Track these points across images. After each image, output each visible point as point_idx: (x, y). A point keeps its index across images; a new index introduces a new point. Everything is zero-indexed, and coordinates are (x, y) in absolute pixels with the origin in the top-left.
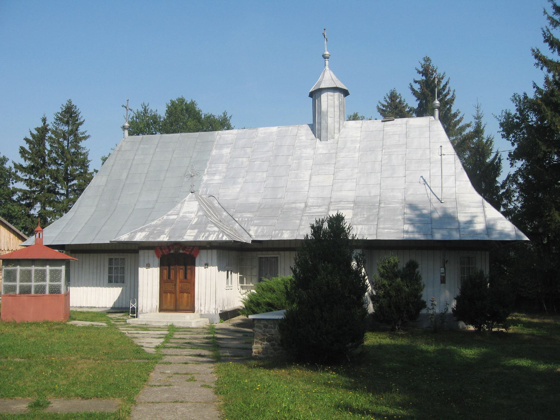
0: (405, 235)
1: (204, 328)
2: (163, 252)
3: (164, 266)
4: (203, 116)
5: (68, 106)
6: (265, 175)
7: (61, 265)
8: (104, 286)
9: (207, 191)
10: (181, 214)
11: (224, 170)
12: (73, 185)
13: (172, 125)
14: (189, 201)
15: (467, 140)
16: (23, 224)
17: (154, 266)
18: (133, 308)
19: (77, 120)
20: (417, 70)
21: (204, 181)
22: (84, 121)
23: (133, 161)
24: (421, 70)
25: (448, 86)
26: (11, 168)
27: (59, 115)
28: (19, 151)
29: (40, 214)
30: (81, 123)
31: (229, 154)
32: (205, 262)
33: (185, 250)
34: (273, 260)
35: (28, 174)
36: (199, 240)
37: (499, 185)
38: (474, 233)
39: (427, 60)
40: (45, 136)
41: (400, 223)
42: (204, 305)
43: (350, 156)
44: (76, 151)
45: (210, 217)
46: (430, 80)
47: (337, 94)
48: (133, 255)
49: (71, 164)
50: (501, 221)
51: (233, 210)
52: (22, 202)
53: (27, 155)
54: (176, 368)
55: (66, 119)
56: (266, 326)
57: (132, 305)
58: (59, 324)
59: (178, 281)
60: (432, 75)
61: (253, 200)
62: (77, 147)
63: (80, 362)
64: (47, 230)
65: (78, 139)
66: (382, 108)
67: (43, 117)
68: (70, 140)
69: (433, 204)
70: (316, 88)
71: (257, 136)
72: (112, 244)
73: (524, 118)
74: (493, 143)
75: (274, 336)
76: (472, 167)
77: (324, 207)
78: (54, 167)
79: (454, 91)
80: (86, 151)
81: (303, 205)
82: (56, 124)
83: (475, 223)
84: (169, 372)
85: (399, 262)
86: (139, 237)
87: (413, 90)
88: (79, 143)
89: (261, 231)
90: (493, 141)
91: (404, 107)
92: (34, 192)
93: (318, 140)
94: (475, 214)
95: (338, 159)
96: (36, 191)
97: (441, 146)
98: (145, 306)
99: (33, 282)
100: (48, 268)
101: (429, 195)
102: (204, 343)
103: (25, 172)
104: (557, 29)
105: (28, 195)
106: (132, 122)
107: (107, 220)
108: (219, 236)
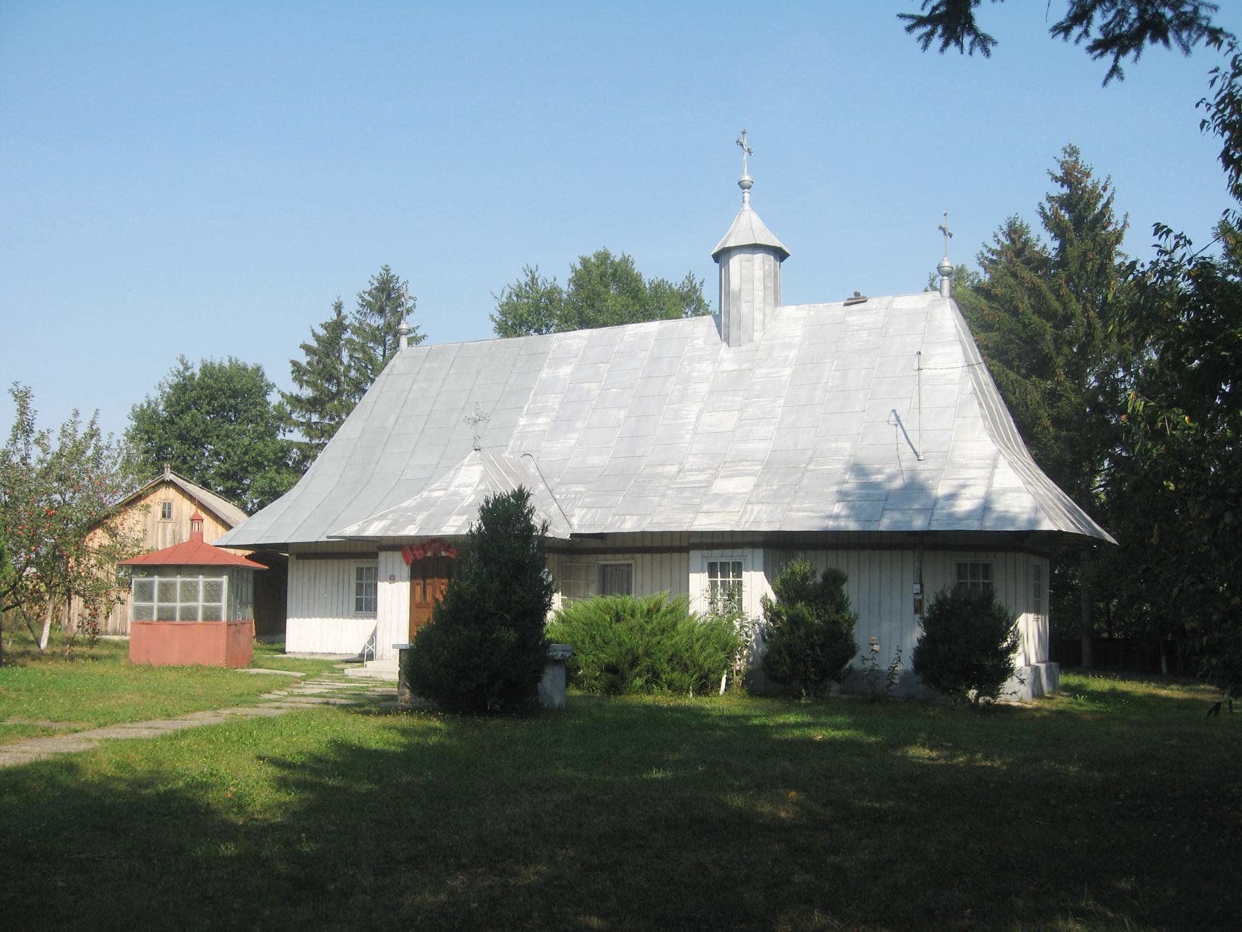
2: (414, 555)
3: (416, 579)
7: (220, 575)
8: (349, 617)
9: (521, 445)
11: (557, 406)
17: (401, 580)
20: (1051, 174)
23: (409, 393)
24: (1059, 173)
32: (390, 573)
33: (448, 551)
34: (626, 570)
39: (1073, 151)
43: (774, 375)
47: (759, 257)
51: (556, 479)
61: (595, 460)
66: (991, 257)
81: (675, 469)
89: (591, 517)
93: (724, 345)
100: (201, 579)
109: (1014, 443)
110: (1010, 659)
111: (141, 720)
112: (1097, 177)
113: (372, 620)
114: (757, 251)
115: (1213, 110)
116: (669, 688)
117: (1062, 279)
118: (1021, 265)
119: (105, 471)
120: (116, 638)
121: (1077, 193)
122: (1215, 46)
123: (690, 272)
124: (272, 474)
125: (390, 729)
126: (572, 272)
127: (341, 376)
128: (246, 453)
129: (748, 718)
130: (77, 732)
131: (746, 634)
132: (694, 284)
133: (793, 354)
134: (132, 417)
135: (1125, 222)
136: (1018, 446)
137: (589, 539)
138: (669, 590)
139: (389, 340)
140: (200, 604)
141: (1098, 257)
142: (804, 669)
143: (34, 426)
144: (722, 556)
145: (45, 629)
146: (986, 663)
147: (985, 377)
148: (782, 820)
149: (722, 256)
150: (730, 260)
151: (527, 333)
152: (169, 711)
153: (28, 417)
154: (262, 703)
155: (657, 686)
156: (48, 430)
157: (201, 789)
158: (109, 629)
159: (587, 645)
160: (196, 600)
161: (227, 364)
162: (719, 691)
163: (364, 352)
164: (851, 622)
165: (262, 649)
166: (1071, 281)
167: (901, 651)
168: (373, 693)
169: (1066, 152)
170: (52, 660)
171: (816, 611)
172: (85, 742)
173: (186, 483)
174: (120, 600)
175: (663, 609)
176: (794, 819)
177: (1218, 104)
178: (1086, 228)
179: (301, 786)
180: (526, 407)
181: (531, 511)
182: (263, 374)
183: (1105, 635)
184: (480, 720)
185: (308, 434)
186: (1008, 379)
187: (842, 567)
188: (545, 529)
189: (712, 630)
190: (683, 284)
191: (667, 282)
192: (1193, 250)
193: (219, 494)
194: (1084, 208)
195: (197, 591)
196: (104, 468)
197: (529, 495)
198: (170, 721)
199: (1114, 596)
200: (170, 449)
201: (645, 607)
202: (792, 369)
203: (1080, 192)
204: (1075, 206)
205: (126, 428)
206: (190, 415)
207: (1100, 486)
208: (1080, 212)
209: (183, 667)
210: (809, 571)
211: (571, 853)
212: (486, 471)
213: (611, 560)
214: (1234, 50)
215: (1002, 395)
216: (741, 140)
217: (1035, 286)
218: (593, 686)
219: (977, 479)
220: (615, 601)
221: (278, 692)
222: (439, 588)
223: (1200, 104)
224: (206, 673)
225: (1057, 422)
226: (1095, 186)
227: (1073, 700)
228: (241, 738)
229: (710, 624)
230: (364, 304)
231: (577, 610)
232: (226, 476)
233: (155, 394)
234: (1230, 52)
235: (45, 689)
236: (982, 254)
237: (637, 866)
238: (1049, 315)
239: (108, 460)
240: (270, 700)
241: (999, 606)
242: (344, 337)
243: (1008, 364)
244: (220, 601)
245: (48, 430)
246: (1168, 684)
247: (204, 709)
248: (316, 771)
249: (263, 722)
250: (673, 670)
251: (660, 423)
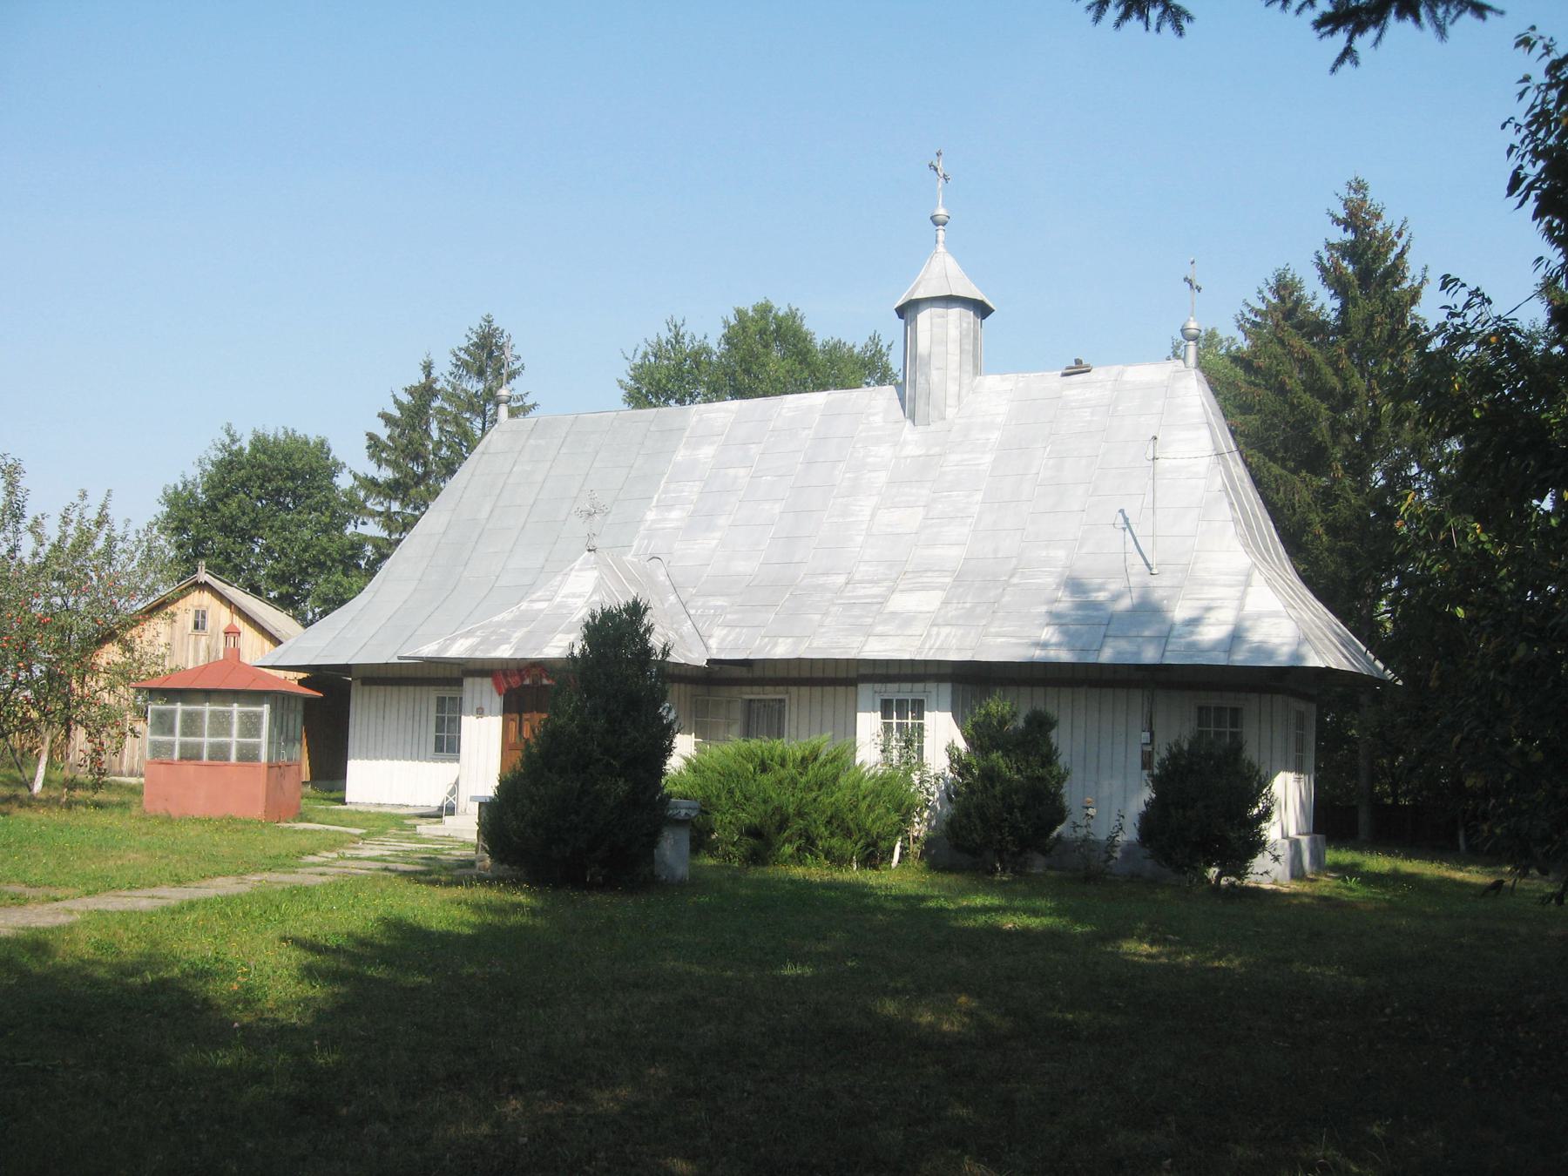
2: (508, 683)
3: (510, 712)
7: (260, 703)
9: (647, 548)
10: (558, 600)
11: (694, 497)
17: (491, 714)
20: (1331, 215)
24: (1342, 214)
32: (477, 705)
34: (777, 706)
39: (1360, 187)
47: (955, 312)
61: (741, 566)
66: (1254, 318)
67: (425, 359)
70: (907, 300)
76: (1457, 471)
81: (841, 579)
86: (458, 649)
93: (909, 423)
100: (236, 709)
109: (1274, 555)
110: (1261, 830)
111: (142, 886)
112: (1390, 219)
113: (456, 763)
114: (954, 305)
115: (1524, 132)
116: (826, 858)
117: (1341, 348)
118: (1290, 329)
119: (119, 568)
120: (133, 780)
121: (1364, 240)
122: (1524, 52)
123: (875, 331)
124: (338, 577)
125: (459, 904)
126: (725, 327)
127: (430, 454)
128: (305, 550)
129: (923, 898)
130: (57, 900)
131: (927, 790)
132: (879, 347)
133: (995, 436)
134: (163, 502)
135: (1424, 278)
136: (1280, 559)
137: (733, 667)
138: (830, 734)
139: (490, 410)
140: (234, 739)
141: (1388, 321)
142: (999, 837)
143: (25, 509)
144: (899, 692)
145: (40, 767)
146: (1231, 834)
147: (1240, 471)
148: (944, 1035)
149: (908, 310)
150: (918, 316)
151: (666, 403)
152: (181, 875)
153: (18, 498)
154: (302, 868)
155: (811, 855)
156: (42, 515)
157: (200, 979)
158: (125, 769)
159: (723, 801)
160: (229, 734)
161: (281, 436)
162: (890, 862)
163: (458, 425)
164: (1061, 779)
165: (316, 798)
166: (1354, 351)
167: (1123, 817)
168: (448, 857)
169: (1351, 187)
170: (44, 806)
172: (65, 914)
173: (225, 586)
174: (134, 732)
175: (822, 758)
176: (959, 1033)
177: (1529, 125)
178: (1374, 285)
179: (333, 976)
180: (655, 500)
181: (649, 630)
182: (329, 449)
183: (1390, 801)
184: (575, 895)
185: (386, 526)
186: (1271, 474)
187: (1051, 709)
188: (666, 652)
189: (883, 785)
190: (866, 347)
191: (844, 344)
192: (1499, 308)
193: (271, 602)
194: (1372, 258)
195: (230, 724)
196: (119, 564)
197: (646, 609)
198: (180, 889)
199: (1399, 751)
200: (210, 542)
201: (799, 755)
202: (994, 456)
203: (1368, 239)
204: (1362, 256)
205: (155, 516)
206: (236, 500)
207: (1386, 612)
208: (1367, 264)
209: (210, 820)
210: (1009, 712)
211: (661, 1073)
212: (602, 578)
213: (759, 694)
214: (1551, 54)
215: (1261, 495)
216: (935, 163)
217: (1306, 357)
218: (730, 853)
219: (1226, 599)
220: (761, 746)
221: (326, 854)
222: (534, 721)
223: (1508, 125)
224: (239, 827)
225: (1332, 529)
226: (1387, 232)
227: (1342, 883)
228: (265, 913)
229: (881, 777)
230: (460, 363)
231: (712, 757)
232: (279, 578)
233: (193, 473)
234: (1546, 57)
235: (26, 844)
236: (1243, 315)
237: (744, 1091)
238: (1325, 394)
239: (124, 554)
240: (314, 864)
241: (1249, 762)
242: (434, 405)
243: (1271, 456)
244: (259, 737)
245: (42, 515)
246: (1466, 865)
247: (225, 874)
248: (355, 958)
249: (295, 893)
250: (832, 835)
251: (824, 520)
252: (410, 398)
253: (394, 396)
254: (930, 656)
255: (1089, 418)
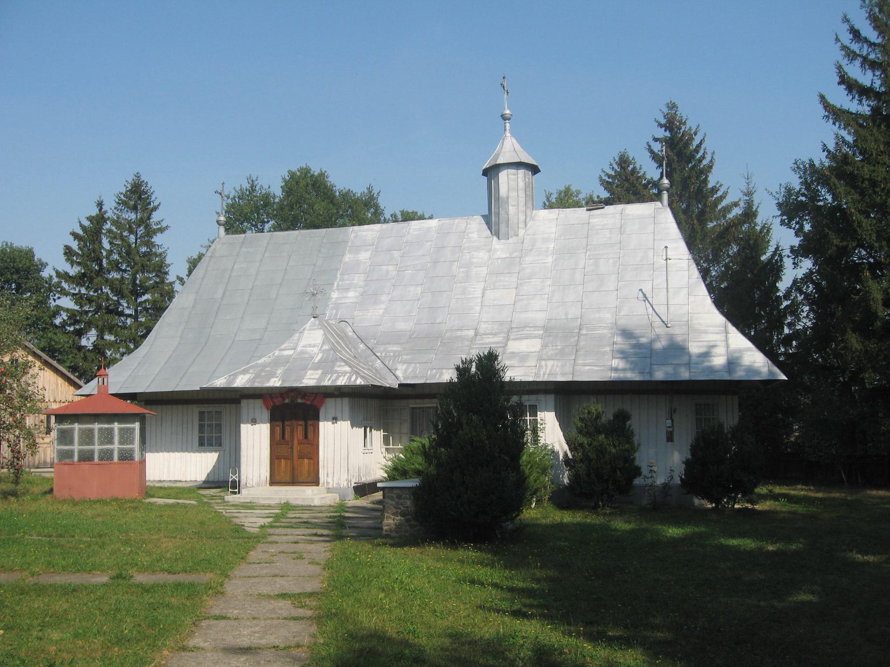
0: (613, 375)
1: (330, 506)
2: (274, 402)
3: (276, 421)
4: (337, 194)
5: (135, 183)
6: (419, 290)
7: (134, 422)
10: (299, 349)
11: (362, 283)
12: (145, 301)
13: (292, 209)
14: (310, 330)
15: (732, 227)
16: (71, 362)
17: (262, 422)
18: (234, 482)
19: (149, 204)
20: (657, 122)
21: (334, 300)
22: (159, 205)
23: (231, 272)
24: (663, 121)
25: (703, 146)
26: (51, 277)
27: (122, 196)
28: (63, 252)
29: (95, 346)
30: (155, 209)
31: (368, 260)
32: (333, 415)
33: (305, 399)
35: (77, 285)
36: (324, 384)
37: (780, 294)
38: (711, 369)
39: (672, 106)
40: (101, 228)
41: (606, 357)
42: (332, 476)
43: (540, 262)
44: (149, 250)
45: (340, 352)
46: (677, 137)
47: (521, 172)
48: (234, 406)
49: (141, 270)
50: (749, 353)
51: (373, 341)
52: (68, 328)
53: (75, 258)
54: (281, 548)
55: (132, 203)
56: (399, 497)
57: (232, 477)
58: (132, 502)
59: (296, 442)
60: (680, 129)
61: (401, 326)
62: (150, 244)
63: (164, 541)
64: (111, 371)
65: (150, 232)
66: (607, 179)
68: (139, 234)
69: (656, 330)
71: (409, 233)
72: (203, 390)
73: (814, 196)
74: (771, 231)
75: (409, 509)
77: (501, 335)
78: (115, 275)
79: (713, 153)
80: (163, 250)
81: (471, 333)
82: (118, 210)
83: (714, 356)
84: (273, 551)
85: (603, 412)
86: (241, 381)
87: (651, 151)
88: (152, 237)
90: (771, 229)
91: (639, 177)
92: (86, 312)
93: (495, 238)
94: (713, 343)
95: (523, 266)
96: (89, 311)
97: (666, 247)
98: (250, 477)
99: (96, 444)
100: (116, 426)
101: (650, 316)
102: (325, 523)
103: (73, 282)
104: (854, 65)
105: (78, 318)
106: (232, 205)
107: (196, 358)
108: (351, 379)
112: (691, 124)
140: (116, 446)
150: (500, 174)
171: (612, 442)
252: (89, 222)
253: (80, 222)
254: (546, 379)
255: (609, 236)
